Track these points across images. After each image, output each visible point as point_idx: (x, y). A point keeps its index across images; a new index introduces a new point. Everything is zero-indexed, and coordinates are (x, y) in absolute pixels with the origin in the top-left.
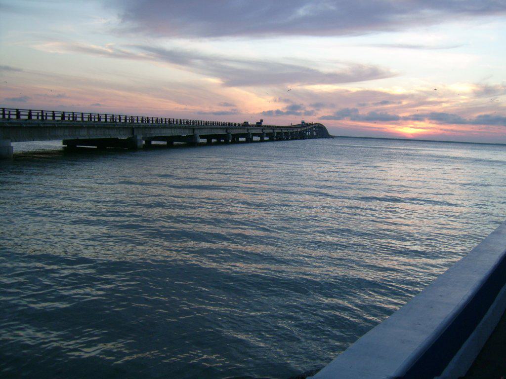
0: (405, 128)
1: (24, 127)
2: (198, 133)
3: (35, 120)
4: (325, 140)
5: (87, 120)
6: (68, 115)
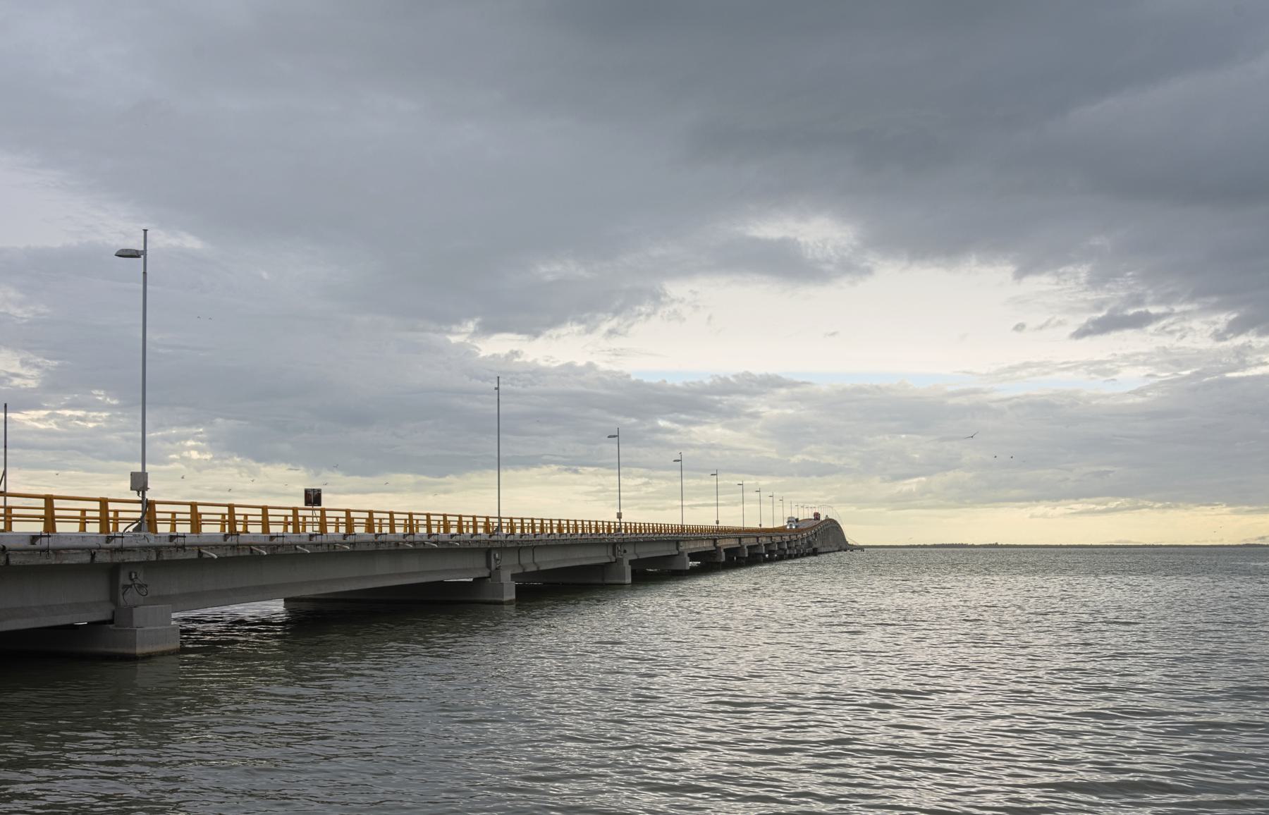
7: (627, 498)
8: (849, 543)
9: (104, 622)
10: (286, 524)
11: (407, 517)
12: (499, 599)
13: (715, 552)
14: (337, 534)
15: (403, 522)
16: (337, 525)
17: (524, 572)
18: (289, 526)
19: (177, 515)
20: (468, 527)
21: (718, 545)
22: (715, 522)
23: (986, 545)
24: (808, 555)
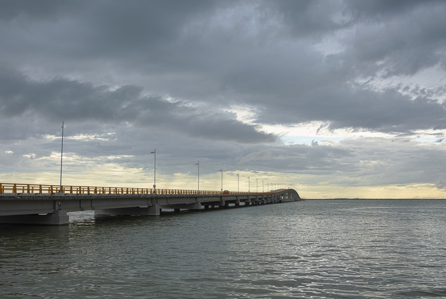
0: (75, 137)
1: (184, 197)
2: (239, 198)
3: (136, 194)
4: (296, 203)
5: (93, 193)
6: (55, 189)
7: (64, 166)
8: (301, 198)
9: (52, 213)
10: (77, 191)
11: (142, 189)
12: (57, 223)
13: (221, 202)
14: (32, 193)
15: (140, 191)
16: (131, 192)
17: (168, 205)
18: (78, 192)
19: (25, 187)
20: (164, 192)
21: (222, 199)
22: (221, 190)
23: (354, 199)
24: (278, 203)
